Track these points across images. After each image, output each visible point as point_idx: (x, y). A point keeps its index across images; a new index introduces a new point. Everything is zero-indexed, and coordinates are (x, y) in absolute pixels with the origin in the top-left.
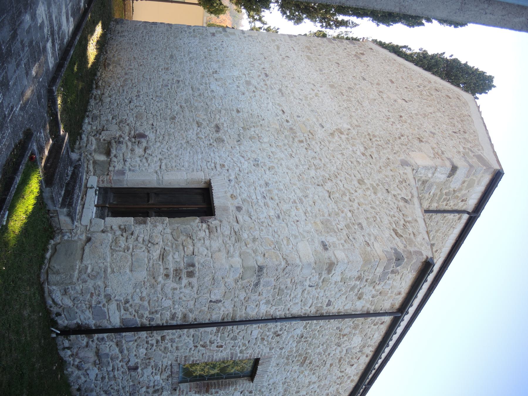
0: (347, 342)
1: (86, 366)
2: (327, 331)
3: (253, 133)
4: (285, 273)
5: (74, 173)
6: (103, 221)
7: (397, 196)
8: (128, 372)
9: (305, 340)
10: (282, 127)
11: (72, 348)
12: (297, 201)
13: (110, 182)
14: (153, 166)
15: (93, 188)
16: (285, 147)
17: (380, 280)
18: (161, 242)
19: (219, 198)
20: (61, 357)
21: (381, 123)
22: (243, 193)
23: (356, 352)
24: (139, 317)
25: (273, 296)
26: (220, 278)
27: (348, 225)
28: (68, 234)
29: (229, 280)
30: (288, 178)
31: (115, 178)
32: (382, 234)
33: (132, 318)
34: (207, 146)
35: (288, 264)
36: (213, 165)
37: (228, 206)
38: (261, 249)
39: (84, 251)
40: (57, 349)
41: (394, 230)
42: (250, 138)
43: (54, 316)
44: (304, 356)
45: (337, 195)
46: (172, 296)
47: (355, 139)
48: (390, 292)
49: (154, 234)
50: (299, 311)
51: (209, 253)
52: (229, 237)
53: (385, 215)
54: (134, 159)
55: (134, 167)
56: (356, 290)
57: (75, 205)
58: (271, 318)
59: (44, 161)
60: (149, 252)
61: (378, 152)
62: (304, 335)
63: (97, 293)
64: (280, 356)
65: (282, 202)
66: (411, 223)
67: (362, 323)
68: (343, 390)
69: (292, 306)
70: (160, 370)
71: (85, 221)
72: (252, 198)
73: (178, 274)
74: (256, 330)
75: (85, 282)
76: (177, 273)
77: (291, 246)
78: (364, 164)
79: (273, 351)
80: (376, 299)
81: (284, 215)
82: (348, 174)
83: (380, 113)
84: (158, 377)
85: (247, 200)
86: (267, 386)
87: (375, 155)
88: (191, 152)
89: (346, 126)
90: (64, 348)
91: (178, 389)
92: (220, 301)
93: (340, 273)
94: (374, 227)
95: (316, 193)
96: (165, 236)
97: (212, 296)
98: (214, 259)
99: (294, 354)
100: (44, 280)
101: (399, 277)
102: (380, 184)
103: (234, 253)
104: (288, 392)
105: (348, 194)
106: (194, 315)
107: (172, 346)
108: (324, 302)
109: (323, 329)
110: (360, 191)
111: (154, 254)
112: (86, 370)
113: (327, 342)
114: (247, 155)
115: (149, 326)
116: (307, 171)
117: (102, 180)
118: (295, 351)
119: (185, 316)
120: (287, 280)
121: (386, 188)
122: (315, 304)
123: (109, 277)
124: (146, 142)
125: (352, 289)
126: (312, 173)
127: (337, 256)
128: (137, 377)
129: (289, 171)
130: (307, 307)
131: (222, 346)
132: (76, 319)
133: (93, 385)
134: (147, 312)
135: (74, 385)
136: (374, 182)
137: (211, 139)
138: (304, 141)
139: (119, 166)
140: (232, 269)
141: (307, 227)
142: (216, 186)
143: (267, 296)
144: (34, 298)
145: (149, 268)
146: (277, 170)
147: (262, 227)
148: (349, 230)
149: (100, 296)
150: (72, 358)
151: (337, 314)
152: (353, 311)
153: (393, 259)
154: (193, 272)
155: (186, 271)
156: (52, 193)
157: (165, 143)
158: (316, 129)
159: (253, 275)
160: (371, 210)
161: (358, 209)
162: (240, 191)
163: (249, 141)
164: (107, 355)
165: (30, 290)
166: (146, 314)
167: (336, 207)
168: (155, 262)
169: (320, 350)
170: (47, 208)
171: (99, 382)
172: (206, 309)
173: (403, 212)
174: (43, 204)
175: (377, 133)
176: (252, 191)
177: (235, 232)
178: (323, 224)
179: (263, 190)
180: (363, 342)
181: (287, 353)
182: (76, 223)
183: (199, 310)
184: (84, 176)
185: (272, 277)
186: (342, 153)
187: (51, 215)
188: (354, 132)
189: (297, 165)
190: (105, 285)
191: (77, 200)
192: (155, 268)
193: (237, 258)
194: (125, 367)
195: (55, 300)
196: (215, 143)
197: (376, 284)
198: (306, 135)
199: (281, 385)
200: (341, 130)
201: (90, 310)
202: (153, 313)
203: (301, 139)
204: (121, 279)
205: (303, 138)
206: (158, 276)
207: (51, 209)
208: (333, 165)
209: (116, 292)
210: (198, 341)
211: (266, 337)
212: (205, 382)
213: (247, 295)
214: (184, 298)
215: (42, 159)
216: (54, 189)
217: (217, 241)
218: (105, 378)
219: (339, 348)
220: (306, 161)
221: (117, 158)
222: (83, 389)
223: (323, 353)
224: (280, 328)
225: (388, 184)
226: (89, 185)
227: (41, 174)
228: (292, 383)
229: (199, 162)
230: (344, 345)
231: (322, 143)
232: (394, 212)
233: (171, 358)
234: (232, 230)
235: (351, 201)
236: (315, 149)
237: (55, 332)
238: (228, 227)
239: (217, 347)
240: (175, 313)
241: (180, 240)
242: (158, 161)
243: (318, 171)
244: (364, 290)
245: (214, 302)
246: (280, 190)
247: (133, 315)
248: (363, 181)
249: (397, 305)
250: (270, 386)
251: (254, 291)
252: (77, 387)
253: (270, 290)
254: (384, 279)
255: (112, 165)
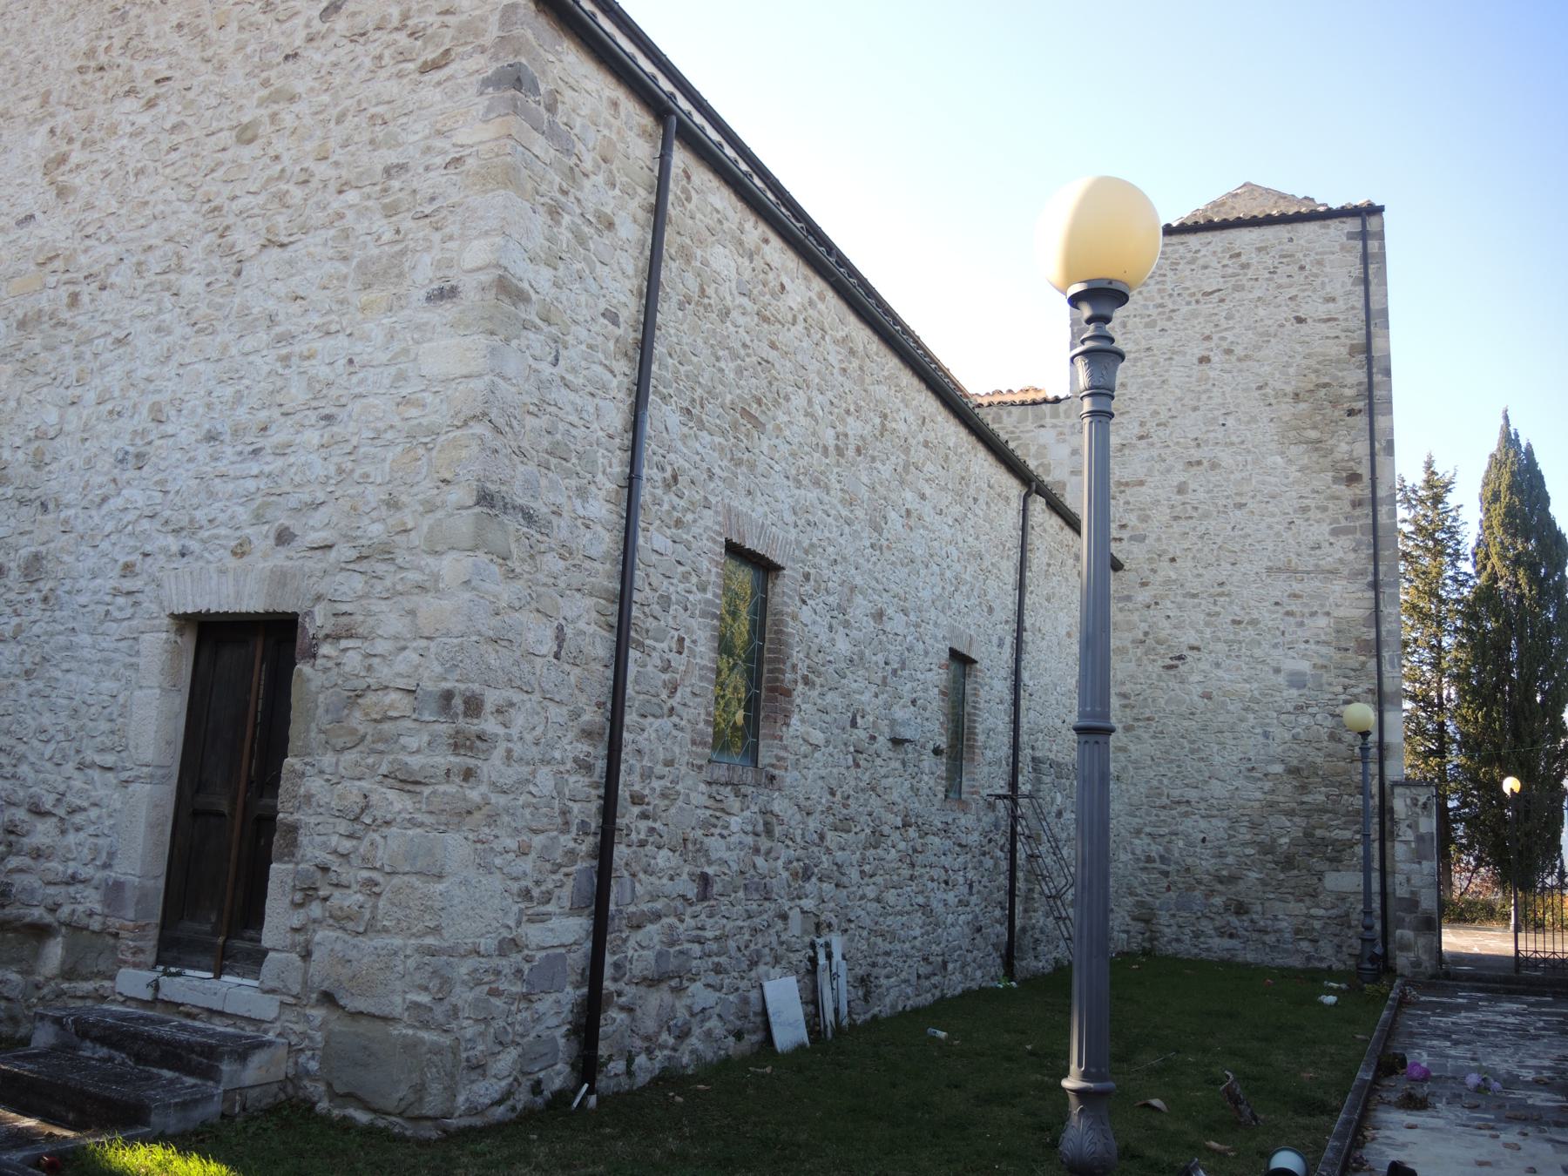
0: (722, 288)
1: (682, 1014)
2: (685, 340)
3: (20, 455)
4: (507, 429)
5: (103, 1040)
6: (271, 954)
7: (313, 30)
8: (712, 902)
9: (698, 407)
10: (12, 355)
11: (630, 1052)
12: (284, 351)
13: (142, 928)
14: (102, 792)
15: (156, 981)
16: (88, 356)
17: (568, 152)
18: (363, 783)
19: (238, 595)
20: (649, 1083)
21: (46, 21)
22: (232, 518)
23: (750, 270)
24: (574, 862)
25: (568, 474)
26: (495, 622)
27: (385, 207)
28: (302, 1059)
29: (506, 596)
30: (201, 367)
31: (131, 914)
32: (432, 109)
33: (572, 883)
34: (49, 613)
35: (485, 414)
36: (121, 600)
37: (272, 571)
38: (426, 488)
39: (361, 1013)
40: (630, 1092)
41: (426, 68)
42: (37, 468)
43: (539, 1100)
44: (738, 415)
45: (281, 220)
46: (528, 764)
47: (91, 120)
48: (606, 132)
49: (333, 804)
50: (618, 409)
51: (415, 644)
52: (374, 581)
53: (369, 83)
54: (70, 851)
55: (99, 853)
56: (586, 229)
57: (212, 1036)
58: (626, 491)
59: (57, 1131)
60: (387, 823)
61: (150, 54)
62: (685, 405)
63: (492, 978)
64: (730, 483)
65: (279, 398)
66: (409, 10)
67: (678, 233)
68: (841, 326)
69: (604, 424)
70: (718, 814)
71: (267, 1008)
72: (253, 490)
73: (468, 743)
74: (653, 540)
75: (455, 1012)
76: (464, 745)
77: (428, 397)
78: (185, 108)
79: (713, 500)
80: (621, 179)
81: (325, 401)
82: (213, 171)
83: (9, 16)
84: (735, 823)
85: (258, 508)
86: (797, 530)
87: (161, 67)
88: (65, 666)
89: (39, 139)
90: (629, 1073)
91: (771, 769)
92: (560, 629)
93: (531, 266)
94: (403, 127)
95: (263, 285)
96: (343, 772)
97: (544, 650)
98: (438, 634)
99: (730, 443)
100: (437, 1128)
101: (568, 93)
102: (264, 75)
103: (427, 572)
104: (822, 478)
105: (284, 187)
106: (586, 707)
107: (661, 777)
108: (604, 331)
109: (678, 348)
110: (279, 146)
111: (398, 806)
112: (692, 1015)
113: (712, 346)
114: (100, 487)
115: (599, 837)
116: (182, 301)
117: (134, 954)
118: (722, 440)
119: (587, 734)
120: (528, 428)
121: (281, 59)
122: (606, 358)
123: (451, 942)
124: (13, 810)
125: (581, 240)
126: (191, 284)
127: (480, 263)
128: (726, 878)
129: (177, 358)
130: (611, 382)
131: (681, 640)
132: (554, 1039)
133: (731, 998)
134: (562, 839)
135: (726, 1049)
136: (253, 91)
137: (26, 597)
138: (72, 288)
139: (91, 900)
140: (473, 583)
141: (373, 335)
142: (198, 600)
143: (566, 493)
144: (488, 1156)
145: (439, 824)
146: (168, 396)
147: (356, 476)
148: (404, 208)
149: (500, 968)
150: (657, 1053)
151: (644, 302)
152: (641, 253)
153: (514, 99)
154: (469, 698)
155: (461, 718)
156: (168, 1106)
157: (21, 748)
158: (35, 242)
159: (501, 523)
160: (346, 124)
161: (337, 164)
162: (222, 524)
163: (50, 472)
164: (660, 955)
165: (466, 1167)
166: (566, 841)
167: (323, 231)
168: (424, 807)
169: (729, 367)
170: (216, 1120)
171: (727, 981)
172: (577, 671)
173: (370, 27)
174: (201, 1133)
175: (82, 44)
176: (231, 487)
177: (360, 558)
178: (370, 286)
179: (229, 451)
180: (729, 245)
181: (725, 463)
182: (271, 1036)
183: (576, 692)
184: (114, 1008)
185: (514, 468)
186: (136, 175)
187: (237, 1109)
188: (64, 117)
189: (158, 330)
190: (471, 953)
191: (196, 1030)
192: (442, 807)
193: (445, 562)
194: (698, 908)
195: (497, 1096)
196: (41, 584)
197: (577, 165)
198: (52, 280)
199: (803, 492)
200: (51, 161)
201: (534, 998)
202: (566, 823)
203: (65, 300)
204: (461, 907)
205: (64, 292)
206: (465, 799)
207: (220, 1108)
208: (174, 213)
209: (495, 924)
210: (659, 705)
211: (675, 514)
212: (763, 696)
213: (553, 550)
214: (539, 731)
215: (51, 1135)
216: (156, 1100)
217: (381, 617)
218: (718, 964)
219: (735, 314)
220: (145, 296)
221: (60, 905)
222: (738, 1023)
223: (739, 362)
224: (655, 470)
225: (264, 50)
226: (147, 995)
227: (103, 1139)
228: (800, 463)
229: (104, 645)
230: (729, 298)
231: (90, 230)
232: (363, 55)
233: (690, 782)
234: (351, 566)
235: (306, 182)
236: (108, 261)
237: (584, 1098)
238: (340, 577)
239: (680, 653)
240: (576, 760)
241: (362, 729)
242: (86, 775)
243: (187, 264)
244: (590, 206)
245: (560, 647)
246: (238, 398)
247: (565, 879)
248: (246, 127)
249: (647, 120)
250: (799, 523)
251: (545, 528)
252: (731, 1039)
253: (551, 481)
254: (569, 139)
255: (85, 921)
